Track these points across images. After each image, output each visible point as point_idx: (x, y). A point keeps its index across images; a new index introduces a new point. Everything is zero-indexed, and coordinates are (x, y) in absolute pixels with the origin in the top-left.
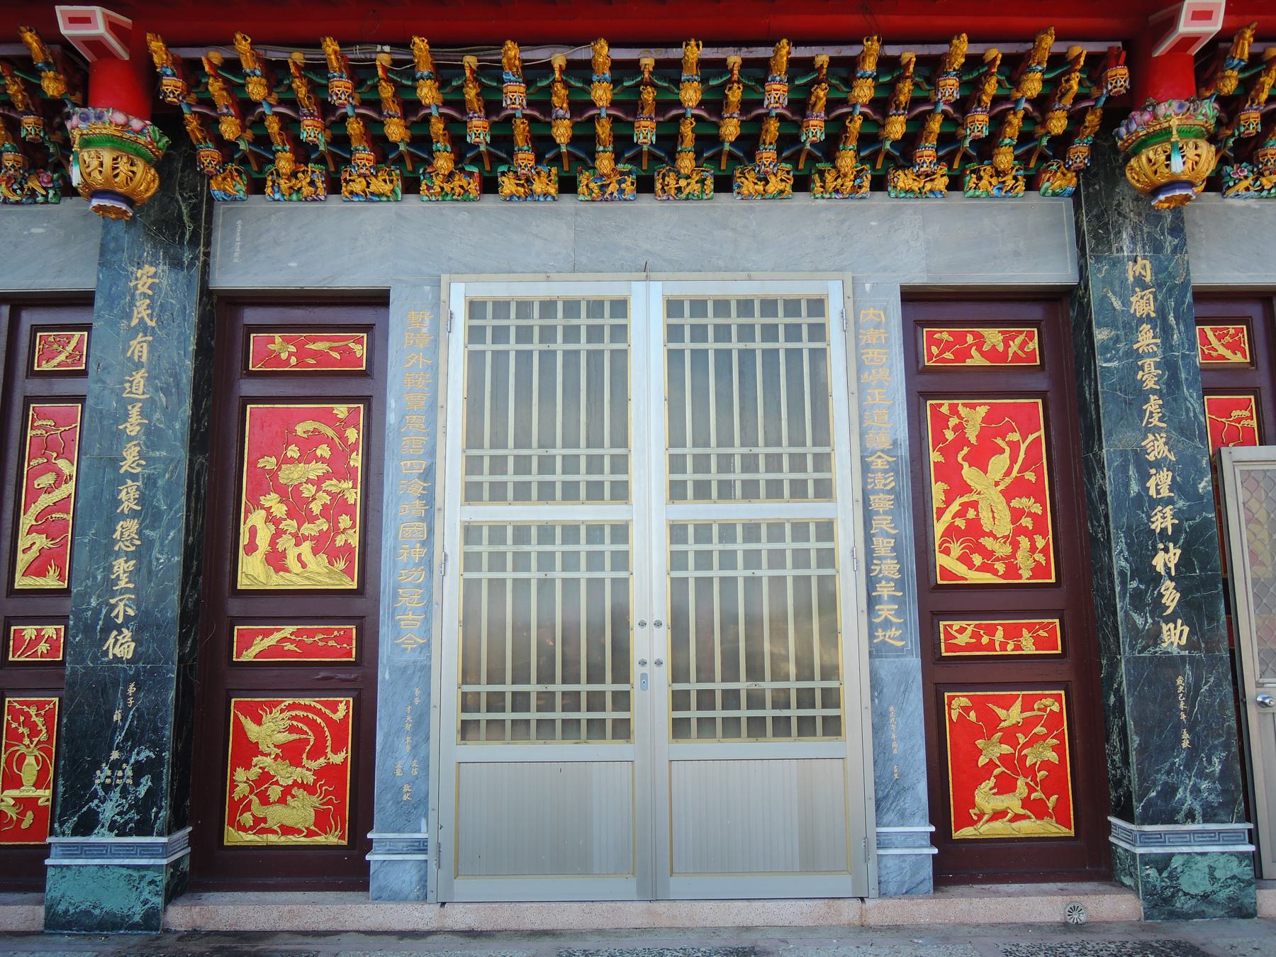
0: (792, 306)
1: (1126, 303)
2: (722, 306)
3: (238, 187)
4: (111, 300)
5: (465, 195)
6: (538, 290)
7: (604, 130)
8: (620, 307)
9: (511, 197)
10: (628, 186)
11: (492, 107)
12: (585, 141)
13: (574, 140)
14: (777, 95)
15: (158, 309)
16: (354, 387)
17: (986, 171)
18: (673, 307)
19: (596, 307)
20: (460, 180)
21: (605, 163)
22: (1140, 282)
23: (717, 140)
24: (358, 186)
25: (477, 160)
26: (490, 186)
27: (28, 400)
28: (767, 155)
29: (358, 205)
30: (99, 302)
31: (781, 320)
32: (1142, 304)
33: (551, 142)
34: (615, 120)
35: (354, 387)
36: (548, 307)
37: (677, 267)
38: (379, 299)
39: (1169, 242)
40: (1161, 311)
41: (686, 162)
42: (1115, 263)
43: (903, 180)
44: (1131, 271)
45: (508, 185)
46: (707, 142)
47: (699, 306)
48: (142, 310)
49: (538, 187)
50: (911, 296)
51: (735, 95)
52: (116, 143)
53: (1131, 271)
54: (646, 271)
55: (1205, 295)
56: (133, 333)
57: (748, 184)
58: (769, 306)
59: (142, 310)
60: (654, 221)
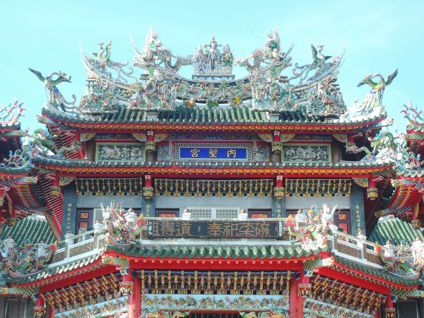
0: (233, 211)
1: (277, 211)
2: (224, 211)
3: (159, 194)
4: (144, 209)
5: (190, 196)
6: (226, 208)
7: (208, 189)
8: (210, 211)
9: (128, 196)
10: (211, 195)
11: (195, 186)
12: (164, 189)
13: (127, 189)
14: (340, 184)
15: (150, 210)
16: (86, 220)
17: (259, 193)
18: (217, 211)
19: (207, 211)
20: (189, 194)
21: (208, 192)
22: (279, 208)
23: (300, 190)
24: (175, 195)
25: (82, 191)
26: (193, 195)
27: (80, 222)
28: (230, 191)
29: (175, 197)
30: (142, 209)
31: (231, 213)
32: (279, 211)
33: (159, 189)
34: (132, 186)
35: (86, 220)
36: (201, 211)
37: (218, 206)
38: (178, 210)
39: (283, 203)
40: (281, 212)
41: (219, 192)
42: (275, 206)
43: (248, 195)
44: (278, 207)
45: (195, 195)
46: (222, 190)
47: (221, 211)
48: (148, 210)
49: (199, 195)
50: (249, 210)
51: (313, 184)
52: (150, 190)
53: (278, 207)
54: (214, 206)
55: (287, 210)
56: (147, 213)
57: (227, 195)
58: (230, 211)
59: (148, 210)
60: (218, 199)
